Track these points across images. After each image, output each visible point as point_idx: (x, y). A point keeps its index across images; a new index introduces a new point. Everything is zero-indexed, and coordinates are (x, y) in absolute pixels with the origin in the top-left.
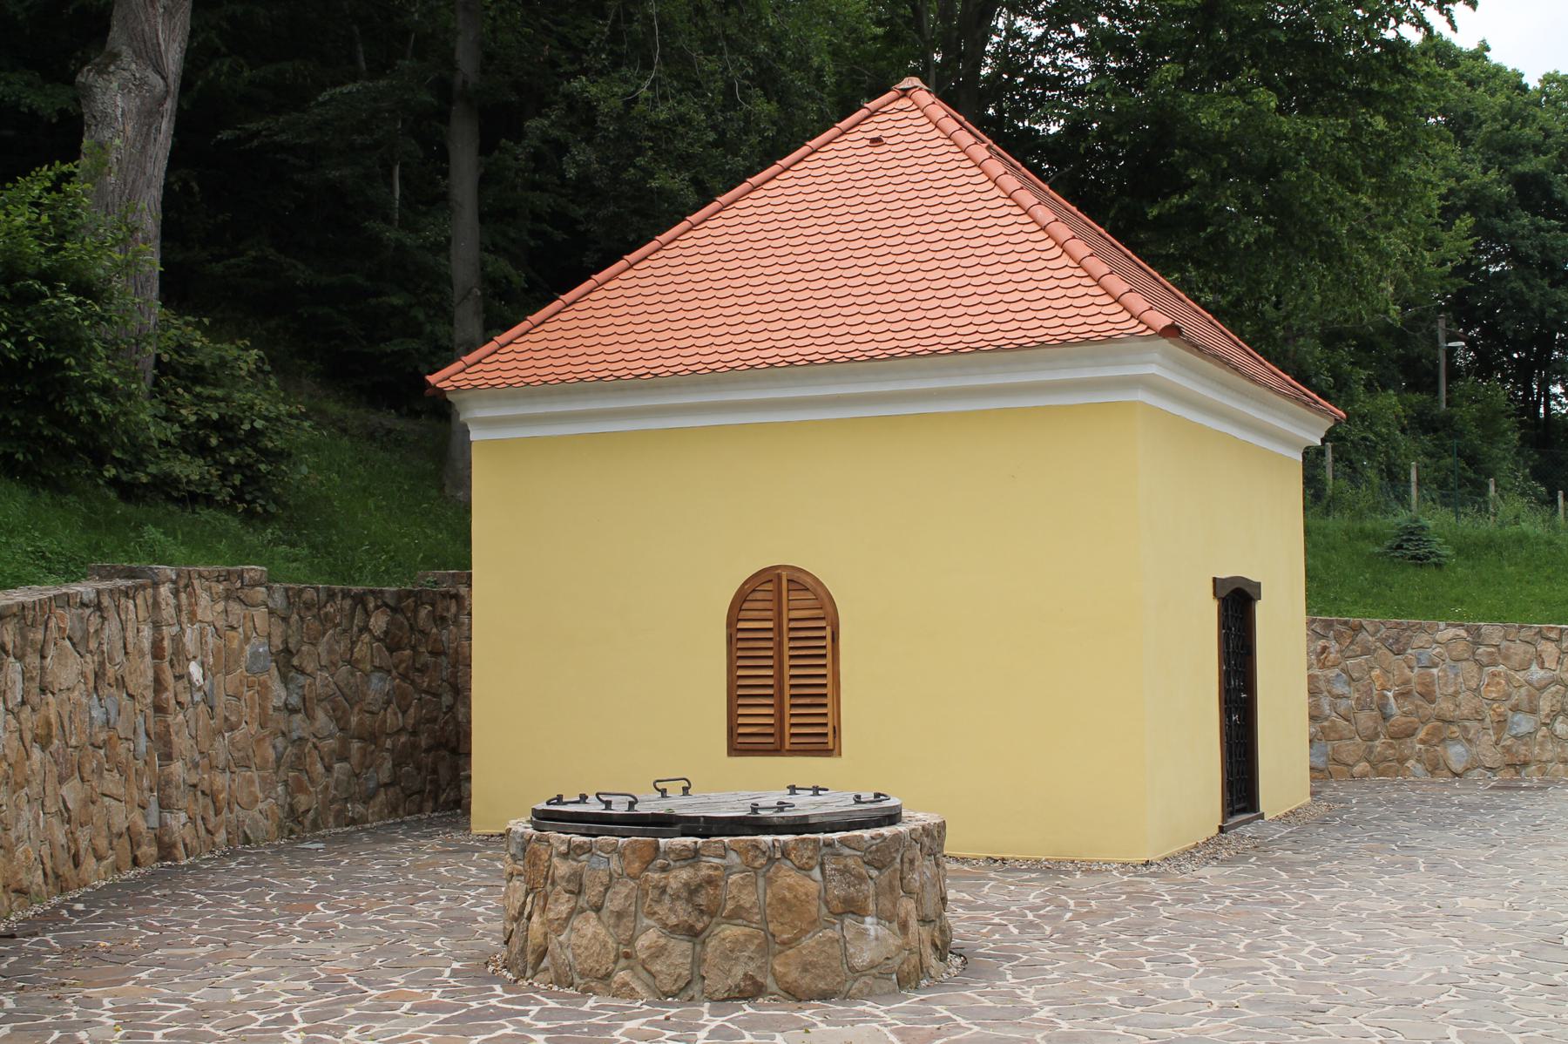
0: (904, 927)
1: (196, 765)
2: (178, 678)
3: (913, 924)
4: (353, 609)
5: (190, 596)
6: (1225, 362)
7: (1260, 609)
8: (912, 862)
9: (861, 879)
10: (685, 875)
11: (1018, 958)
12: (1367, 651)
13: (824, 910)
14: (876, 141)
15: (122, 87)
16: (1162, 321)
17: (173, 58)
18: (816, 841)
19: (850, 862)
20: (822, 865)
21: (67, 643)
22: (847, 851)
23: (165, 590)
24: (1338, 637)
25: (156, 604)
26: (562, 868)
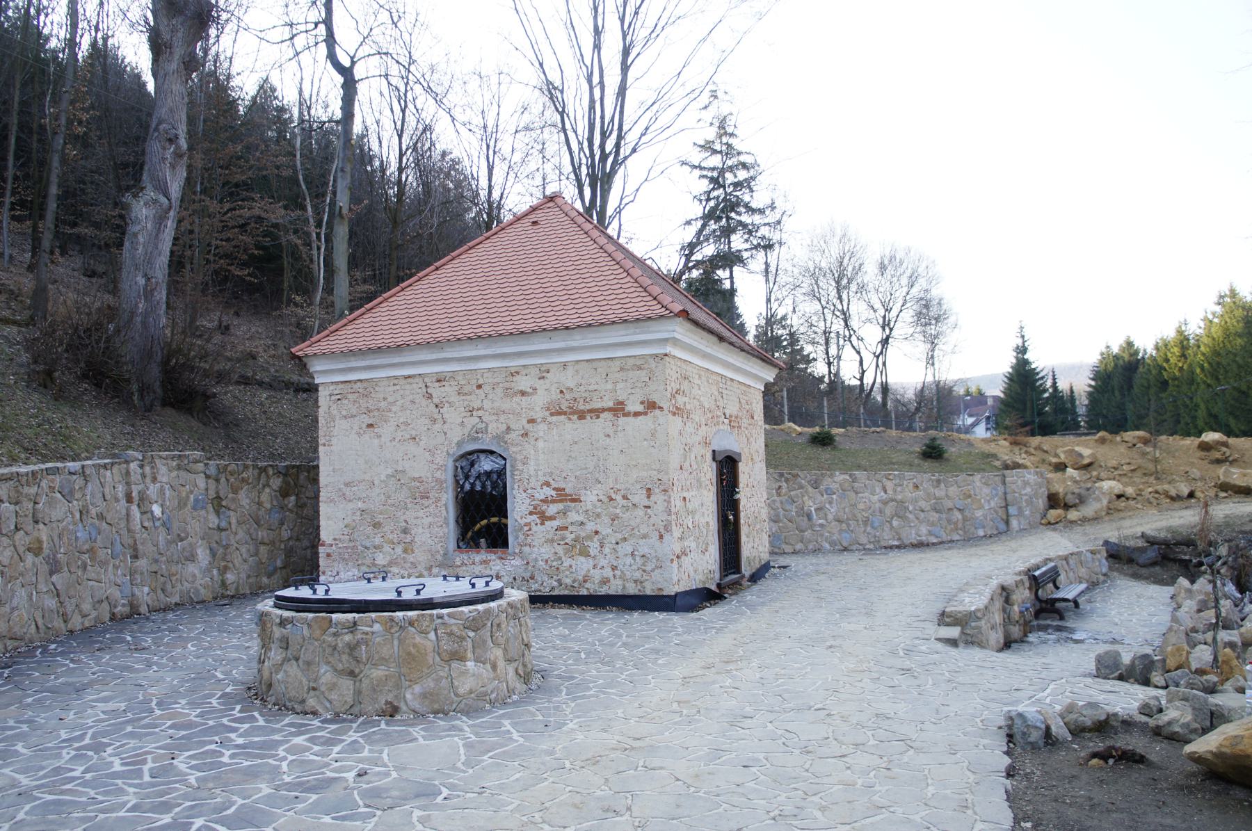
0: (494, 667)
1: (156, 561)
2: (143, 513)
3: (501, 664)
4: (260, 475)
5: (152, 468)
6: (711, 331)
7: (742, 467)
8: (499, 625)
9: (462, 638)
10: (347, 638)
11: (574, 678)
12: (801, 487)
13: (437, 659)
14: (535, 223)
15: (145, 204)
16: (677, 308)
17: (175, 189)
18: (431, 615)
19: (455, 629)
20: (436, 630)
21: (59, 495)
22: (453, 621)
23: (133, 466)
24: (787, 480)
25: (128, 473)
26: (278, 632)
